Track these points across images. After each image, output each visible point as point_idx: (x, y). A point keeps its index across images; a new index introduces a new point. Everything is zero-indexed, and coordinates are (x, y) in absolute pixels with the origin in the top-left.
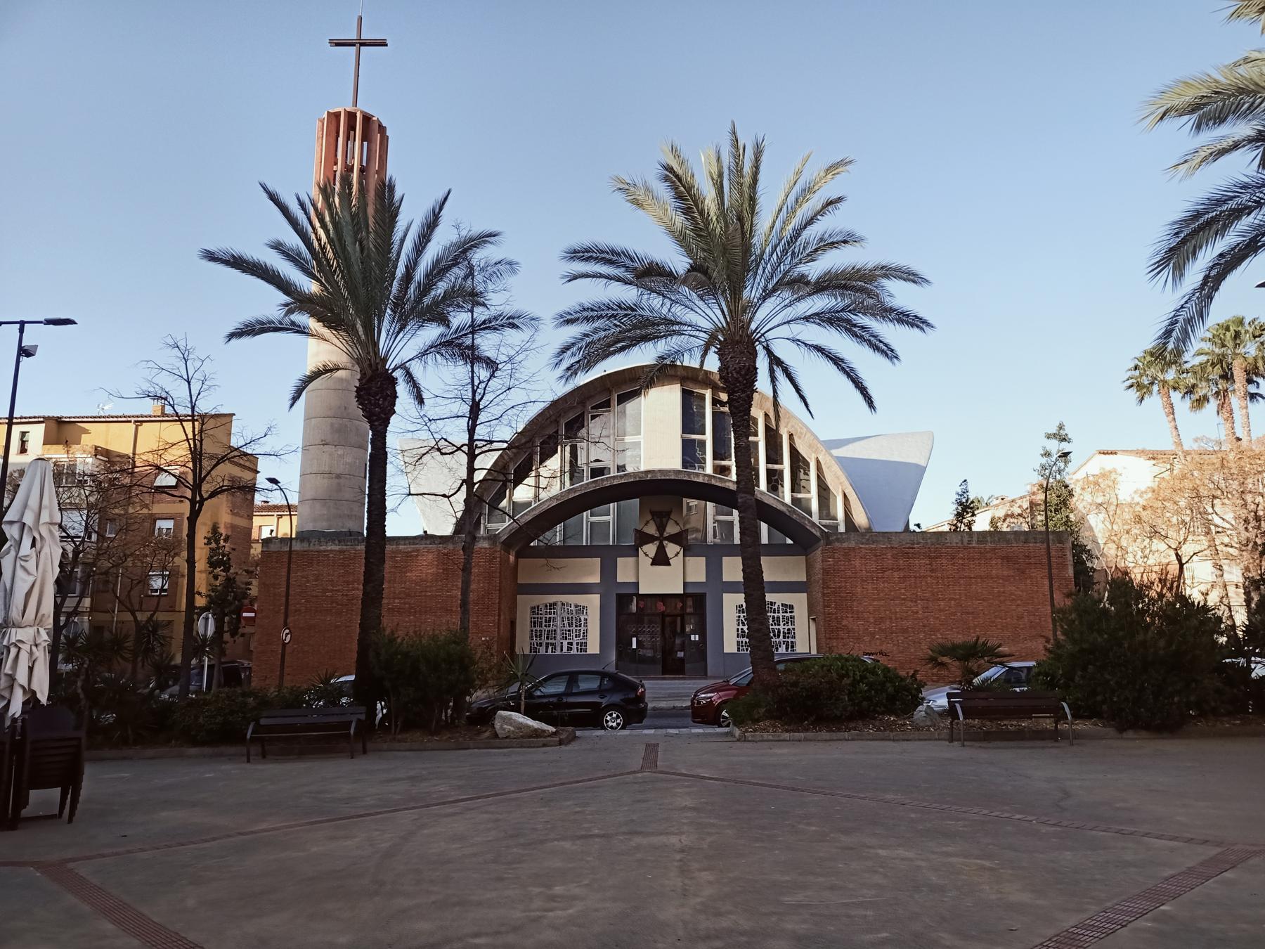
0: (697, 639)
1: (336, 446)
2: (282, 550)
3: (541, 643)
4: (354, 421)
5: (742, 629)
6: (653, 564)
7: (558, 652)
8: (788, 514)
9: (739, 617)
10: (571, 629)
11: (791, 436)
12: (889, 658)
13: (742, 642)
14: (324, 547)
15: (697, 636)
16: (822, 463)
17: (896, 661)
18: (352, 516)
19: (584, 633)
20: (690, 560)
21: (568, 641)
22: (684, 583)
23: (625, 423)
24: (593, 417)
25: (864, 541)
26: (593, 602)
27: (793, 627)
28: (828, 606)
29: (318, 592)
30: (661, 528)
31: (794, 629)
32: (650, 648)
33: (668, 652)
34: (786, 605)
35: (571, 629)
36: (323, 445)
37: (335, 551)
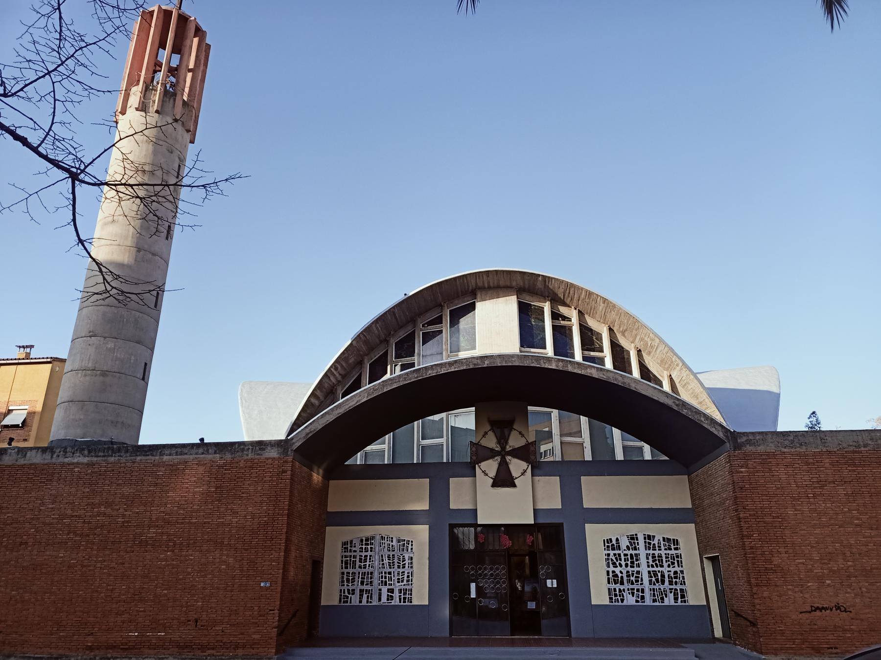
0: (555, 585)
1: (105, 338)
2: (18, 463)
3: (353, 590)
4: (133, 312)
5: (613, 572)
6: (494, 485)
7: (375, 602)
8: (675, 408)
9: (609, 555)
10: (392, 570)
11: (639, 351)
12: (851, 615)
13: (615, 590)
14: (70, 459)
15: (555, 581)
16: (677, 381)
17: (862, 620)
18: (117, 422)
19: (408, 577)
20: (541, 480)
21: (388, 587)
22: (534, 509)
23: (458, 338)
24: (427, 338)
25: (787, 442)
26: (421, 533)
27: (680, 569)
28: (749, 536)
29: (53, 518)
30: (503, 440)
31: (682, 572)
32: (494, 597)
33: (516, 598)
34: (669, 540)
35: (392, 570)
36: (90, 337)
37: (82, 464)
